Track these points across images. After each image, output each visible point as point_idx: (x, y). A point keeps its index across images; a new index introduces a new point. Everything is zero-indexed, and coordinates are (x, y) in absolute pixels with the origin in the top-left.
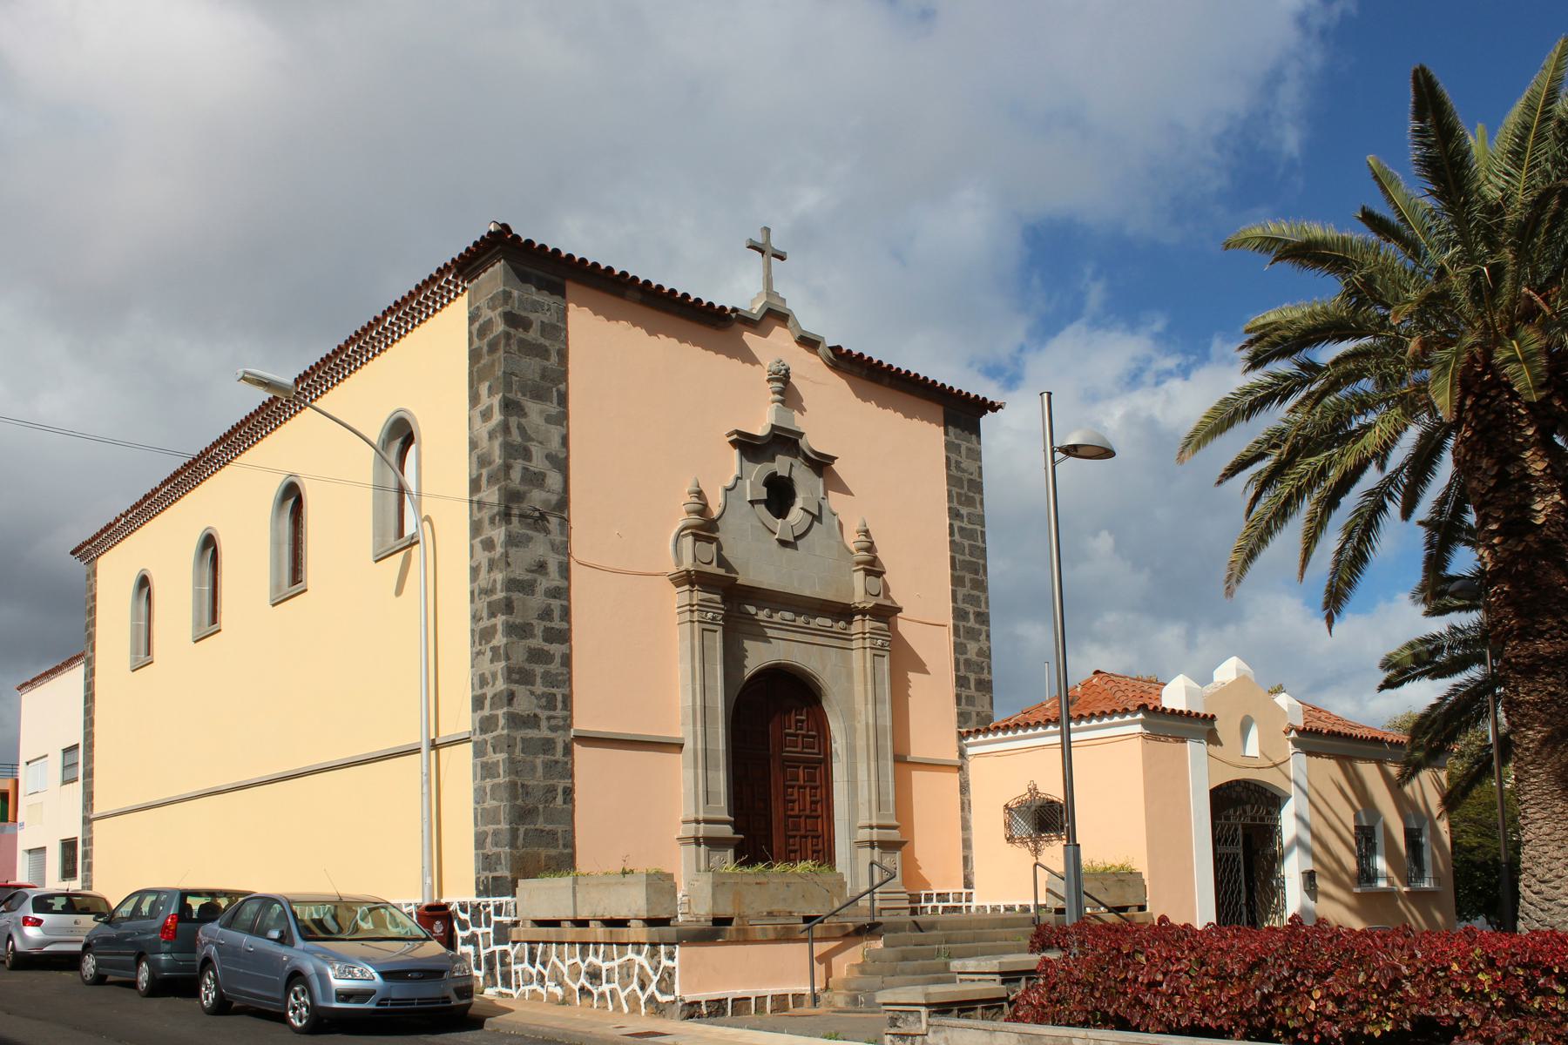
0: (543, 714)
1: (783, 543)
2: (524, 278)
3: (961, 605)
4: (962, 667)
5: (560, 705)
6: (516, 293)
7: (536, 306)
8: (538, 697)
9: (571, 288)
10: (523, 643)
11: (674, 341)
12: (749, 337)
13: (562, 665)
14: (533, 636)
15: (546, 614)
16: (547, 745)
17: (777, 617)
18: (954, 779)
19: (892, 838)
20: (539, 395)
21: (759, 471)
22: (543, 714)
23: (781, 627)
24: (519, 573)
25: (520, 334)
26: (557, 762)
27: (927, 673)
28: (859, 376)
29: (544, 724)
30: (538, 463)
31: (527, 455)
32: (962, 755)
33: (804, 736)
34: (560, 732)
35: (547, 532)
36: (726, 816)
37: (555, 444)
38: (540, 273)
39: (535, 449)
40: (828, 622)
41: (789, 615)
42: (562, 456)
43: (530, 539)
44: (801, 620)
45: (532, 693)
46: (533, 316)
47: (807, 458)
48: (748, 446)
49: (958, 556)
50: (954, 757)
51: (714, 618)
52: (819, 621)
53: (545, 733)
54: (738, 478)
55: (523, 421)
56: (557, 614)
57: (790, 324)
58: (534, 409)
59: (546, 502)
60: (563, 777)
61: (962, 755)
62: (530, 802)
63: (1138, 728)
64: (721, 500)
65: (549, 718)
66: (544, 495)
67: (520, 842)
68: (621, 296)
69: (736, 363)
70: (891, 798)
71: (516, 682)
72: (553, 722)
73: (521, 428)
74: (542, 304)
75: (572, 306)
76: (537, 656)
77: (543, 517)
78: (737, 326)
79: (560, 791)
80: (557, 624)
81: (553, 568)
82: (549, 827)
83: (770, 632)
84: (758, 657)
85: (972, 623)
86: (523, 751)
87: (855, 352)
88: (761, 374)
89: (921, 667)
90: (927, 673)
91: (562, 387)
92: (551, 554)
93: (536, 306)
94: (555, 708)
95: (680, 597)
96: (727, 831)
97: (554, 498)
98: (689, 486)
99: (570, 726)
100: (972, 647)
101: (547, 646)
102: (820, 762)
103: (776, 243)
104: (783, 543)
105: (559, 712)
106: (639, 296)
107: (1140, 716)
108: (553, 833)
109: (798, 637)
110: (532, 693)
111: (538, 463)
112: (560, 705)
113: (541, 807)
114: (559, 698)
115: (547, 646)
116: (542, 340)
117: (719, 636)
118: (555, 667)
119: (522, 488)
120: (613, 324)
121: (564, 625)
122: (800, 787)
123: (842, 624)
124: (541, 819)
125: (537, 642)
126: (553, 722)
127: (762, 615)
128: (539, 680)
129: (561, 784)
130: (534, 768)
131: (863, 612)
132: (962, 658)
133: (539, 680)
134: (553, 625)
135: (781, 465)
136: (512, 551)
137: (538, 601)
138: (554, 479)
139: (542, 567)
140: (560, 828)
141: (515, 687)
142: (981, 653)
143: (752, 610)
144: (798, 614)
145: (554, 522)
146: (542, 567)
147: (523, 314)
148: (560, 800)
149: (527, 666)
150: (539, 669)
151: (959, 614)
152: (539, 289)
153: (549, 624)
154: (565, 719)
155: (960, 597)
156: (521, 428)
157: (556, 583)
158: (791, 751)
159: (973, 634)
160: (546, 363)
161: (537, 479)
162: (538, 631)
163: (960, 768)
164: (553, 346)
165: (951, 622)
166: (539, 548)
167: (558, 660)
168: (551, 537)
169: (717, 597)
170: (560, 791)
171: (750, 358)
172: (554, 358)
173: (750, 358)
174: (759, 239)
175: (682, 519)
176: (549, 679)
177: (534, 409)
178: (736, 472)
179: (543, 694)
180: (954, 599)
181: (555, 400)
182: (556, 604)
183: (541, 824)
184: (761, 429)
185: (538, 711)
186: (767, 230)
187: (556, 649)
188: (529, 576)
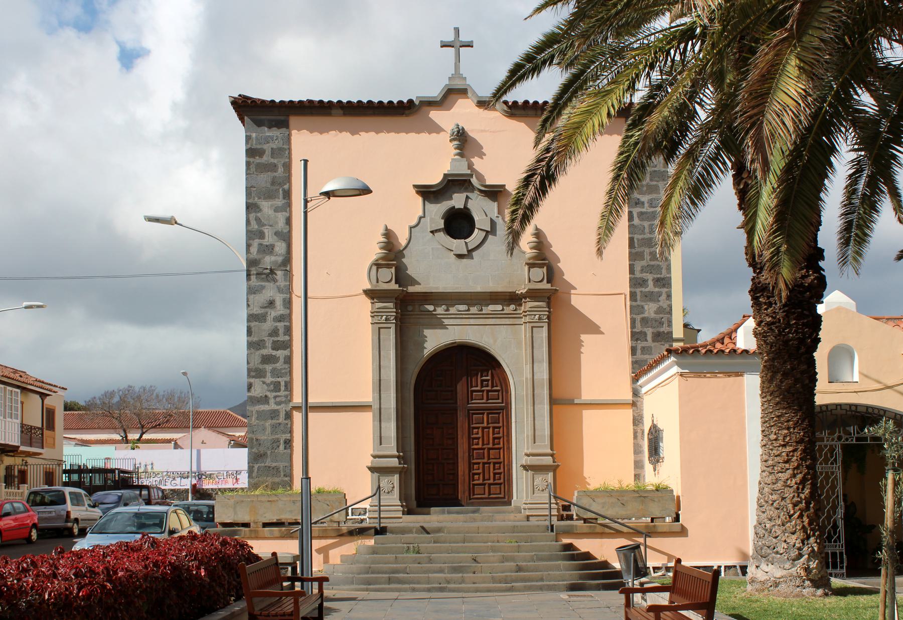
0: (271, 395)
1: (460, 256)
2: (259, 124)
3: (638, 274)
4: (638, 324)
5: (283, 388)
6: (254, 135)
7: (267, 140)
8: (268, 385)
9: (293, 120)
10: (258, 353)
11: (372, 134)
12: (435, 115)
13: (285, 363)
14: (264, 347)
15: (274, 332)
16: (274, 414)
17: (453, 310)
18: (628, 413)
19: (544, 463)
20: (269, 195)
21: (438, 210)
22: (271, 395)
23: (456, 316)
24: (256, 310)
25: (258, 160)
26: (280, 424)
27: (602, 333)
28: (527, 116)
29: (272, 401)
30: (269, 239)
31: (261, 235)
32: (636, 393)
33: (488, 391)
34: (283, 405)
35: (275, 281)
36: (396, 453)
37: (281, 224)
38: (268, 117)
39: (267, 231)
40: (499, 307)
41: (463, 307)
42: (285, 231)
43: (263, 287)
44: (474, 310)
45: (264, 383)
46: (265, 147)
47: (481, 191)
48: (428, 193)
49: (636, 236)
50: (629, 397)
51: (540, 319)
52: (491, 307)
53: (272, 406)
54: (420, 218)
55: (259, 215)
56: (281, 331)
57: (470, 94)
58: (266, 206)
59: (275, 262)
60: (284, 433)
61: (636, 393)
62: (262, 450)
63: (675, 369)
64: (407, 235)
65: (275, 397)
66: (273, 258)
67: (254, 475)
68: (329, 115)
69: (424, 136)
70: (547, 432)
71: (253, 377)
72: (278, 399)
73: (258, 220)
74: (272, 138)
75: (294, 132)
76: (267, 359)
77: (272, 271)
78: (426, 109)
79: (282, 442)
80: (282, 338)
81: (279, 303)
82: (274, 464)
83: (446, 322)
84: (434, 340)
85: (651, 287)
86: (257, 419)
87: (386, 101)
88: (445, 137)
89: (594, 329)
90: (602, 333)
91: (286, 187)
92: (278, 295)
93: (267, 140)
94: (279, 390)
95: (366, 305)
96: (394, 462)
97: (280, 259)
98: (382, 230)
99: (290, 401)
100: (650, 309)
101: (274, 353)
102: (502, 409)
103: (463, 38)
104: (460, 256)
105: (282, 393)
106: (341, 112)
107: (672, 359)
108: (277, 469)
109: (472, 321)
110: (264, 383)
111: (269, 239)
112: (283, 388)
113: (269, 452)
114: (283, 384)
115: (274, 353)
116: (272, 160)
117: (392, 331)
118: (279, 365)
119: (260, 256)
120: (325, 136)
121: (287, 338)
122: (483, 428)
123: (512, 307)
124: (269, 460)
125: (268, 351)
126: (278, 399)
127: (440, 310)
128: (269, 374)
129: (284, 437)
130: (264, 429)
131: (523, 296)
132: (638, 318)
133: (269, 374)
134: (279, 339)
135: (457, 201)
136: (251, 297)
137: (269, 325)
138: (280, 247)
139: (271, 304)
140: (281, 465)
141: (252, 380)
142: (660, 310)
143: (431, 308)
144: (469, 305)
145: (280, 274)
146: (271, 304)
147: (259, 147)
148: (282, 447)
149: (261, 367)
150: (269, 368)
151: (636, 282)
152: (270, 127)
153: (276, 339)
154: (286, 396)
155: (638, 268)
156: (258, 220)
157: (282, 312)
158: (476, 403)
159: (651, 297)
160: (275, 174)
161: (269, 249)
162: (269, 344)
163: (634, 404)
164: (279, 162)
165: (627, 291)
166: (270, 292)
167: (282, 360)
168: (278, 284)
169: (391, 305)
170: (282, 442)
171: (436, 129)
172: (281, 170)
173: (436, 129)
174: (450, 37)
175: (375, 252)
176: (276, 373)
177: (266, 206)
178: (421, 214)
179: (272, 382)
180: (632, 271)
181: (281, 196)
182: (281, 325)
183: (268, 463)
184: (434, 179)
185: (268, 394)
186: (457, 30)
187: (638, 328)
188: (263, 311)
